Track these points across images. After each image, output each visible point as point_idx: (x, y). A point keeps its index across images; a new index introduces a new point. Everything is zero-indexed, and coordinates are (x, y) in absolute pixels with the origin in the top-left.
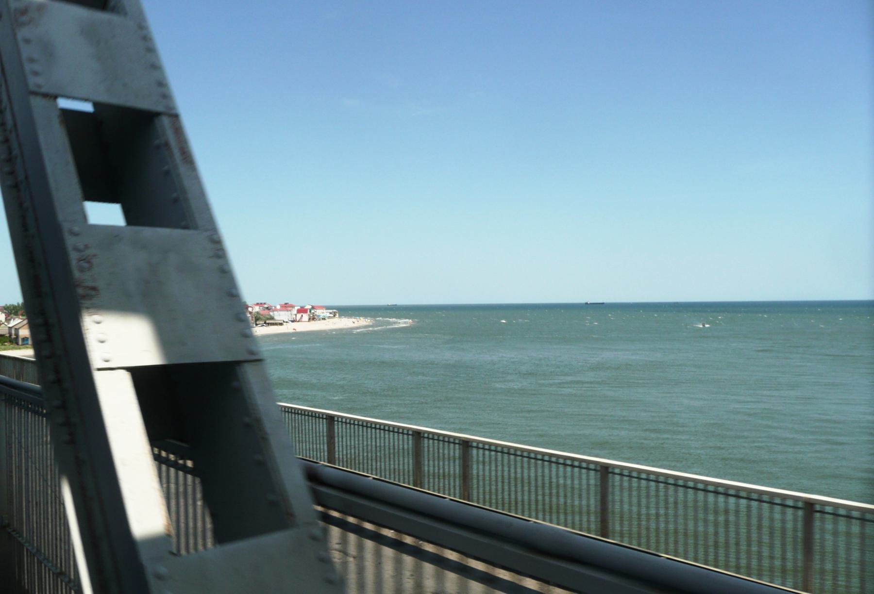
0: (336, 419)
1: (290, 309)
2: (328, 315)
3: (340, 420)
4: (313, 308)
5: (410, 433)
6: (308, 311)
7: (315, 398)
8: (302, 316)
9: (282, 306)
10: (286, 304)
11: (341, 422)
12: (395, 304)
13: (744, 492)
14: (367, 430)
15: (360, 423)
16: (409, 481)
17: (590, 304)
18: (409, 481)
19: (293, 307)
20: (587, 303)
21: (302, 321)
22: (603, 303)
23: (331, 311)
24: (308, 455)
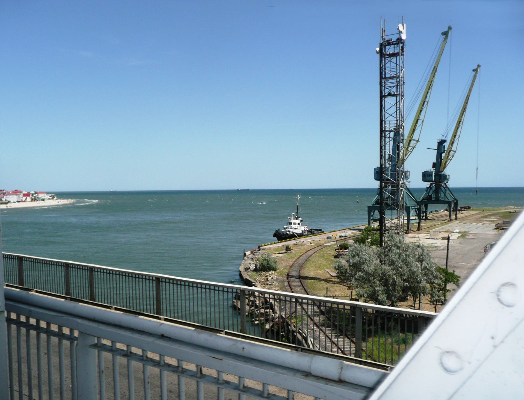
0: (24, 259)
1: (18, 193)
2: (48, 197)
3: (60, 264)
4: (36, 193)
5: (63, 264)
6: (31, 195)
7: (380, 290)
8: (26, 198)
9: (13, 192)
10: (16, 190)
11: (124, 276)
12: (115, 190)
13: (342, 305)
14: (59, 267)
15: (108, 272)
16: (51, 290)
17: (240, 190)
18: (51, 290)
19: (21, 192)
20: (238, 190)
21: (26, 202)
22: (248, 190)
23: (50, 195)
24: (222, 324)
